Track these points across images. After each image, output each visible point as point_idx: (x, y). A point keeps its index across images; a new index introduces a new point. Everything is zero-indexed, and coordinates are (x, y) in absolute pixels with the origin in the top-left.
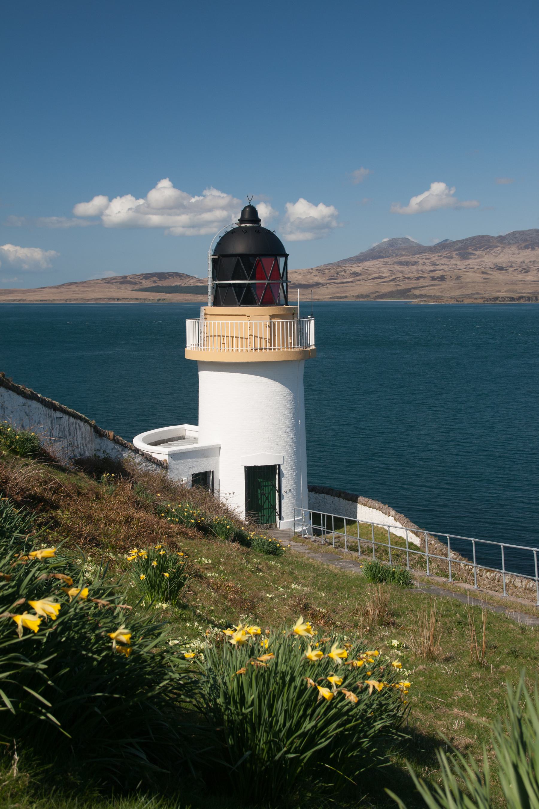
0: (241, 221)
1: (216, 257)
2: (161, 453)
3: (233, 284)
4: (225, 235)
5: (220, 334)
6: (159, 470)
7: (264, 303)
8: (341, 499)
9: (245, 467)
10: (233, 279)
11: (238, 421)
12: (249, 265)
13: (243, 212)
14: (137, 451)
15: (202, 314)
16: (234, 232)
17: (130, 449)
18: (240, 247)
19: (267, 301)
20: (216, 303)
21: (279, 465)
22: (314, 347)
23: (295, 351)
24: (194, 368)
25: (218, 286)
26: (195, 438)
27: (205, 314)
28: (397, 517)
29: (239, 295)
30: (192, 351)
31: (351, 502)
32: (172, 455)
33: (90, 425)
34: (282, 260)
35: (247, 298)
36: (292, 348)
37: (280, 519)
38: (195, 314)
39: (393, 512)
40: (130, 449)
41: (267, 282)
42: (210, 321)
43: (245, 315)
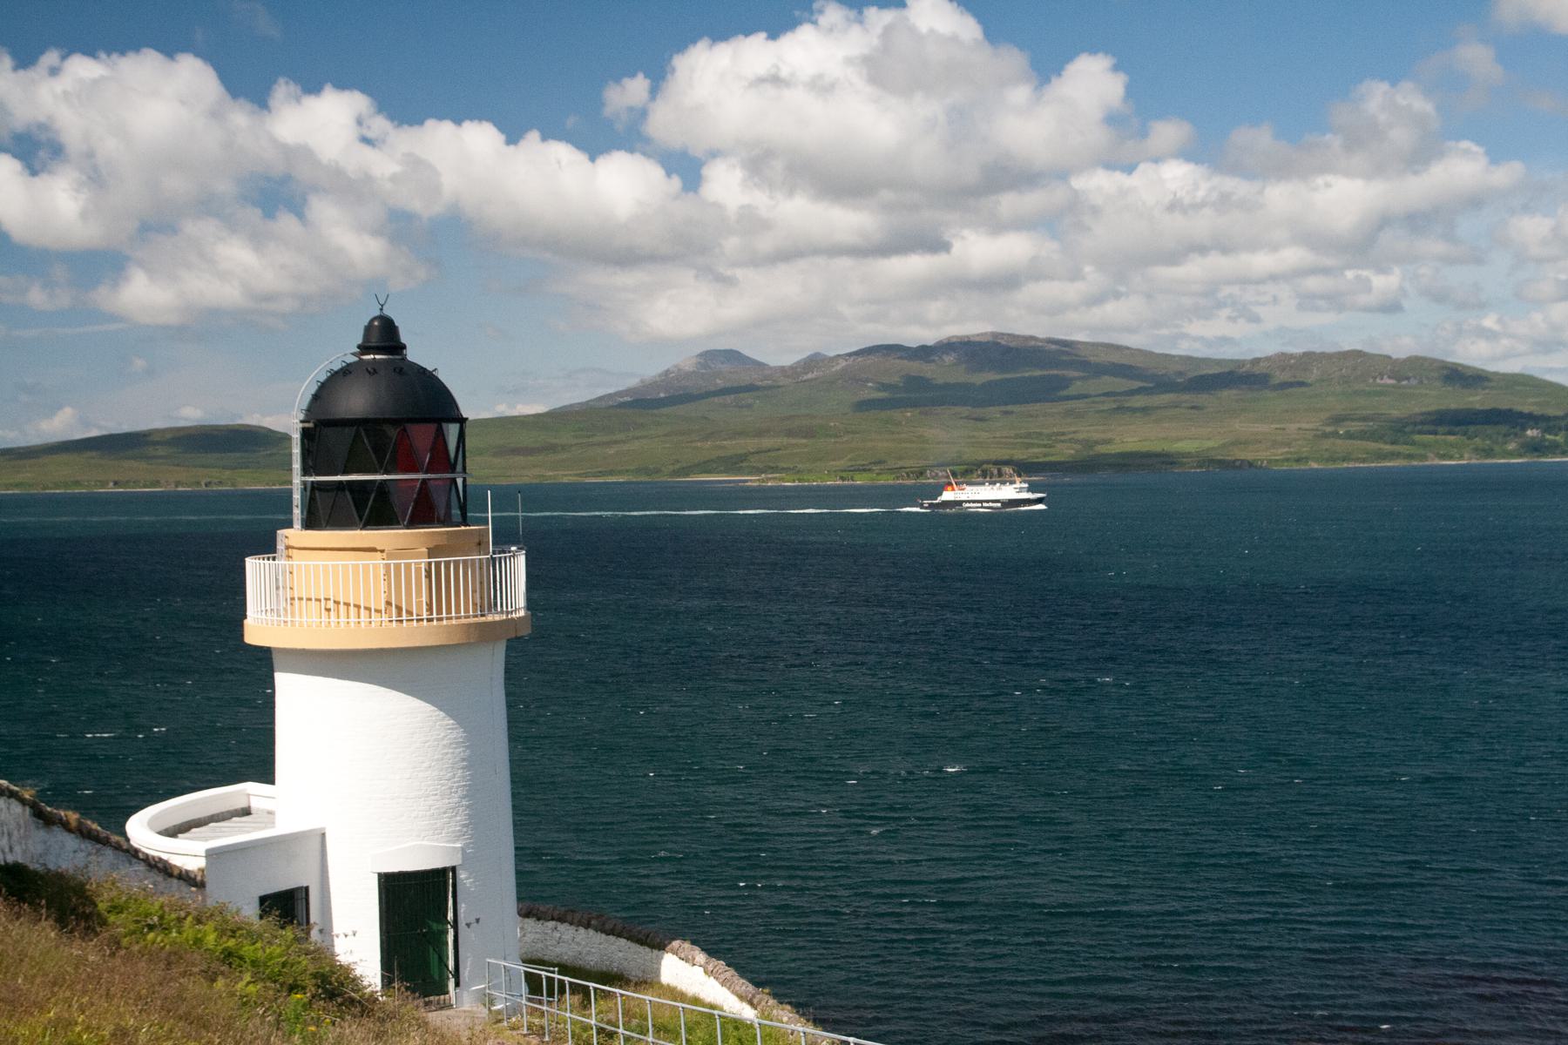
0: (364, 348)
1: (310, 425)
2: (188, 854)
3: (348, 482)
4: (329, 380)
5: (311, 589)
6: (190, 896)
7: (412, 524)
8: (591, 932)
9: (380, 875)
10: (345, 473)
11: (359, 777)
12: (386, 443)
13: (368, 329)
14: (134, 854)
15: (280, 546)
16: (346, 371)
17: (117, 847)
18: (356, 402)
19: (423, 513)
20: (310, 523)
21: (454, 869)
22: (522, 613)
23: (469, 625)
24: (263, 662)
25: (316, 487)
26: (270, 813)
27: (288, 547)
28: (710, 968)
29: (360, 506)
30: (259, 629)
31: (611, 937)
32: (211, 854)
33: (23, 801)
34: (452, 431)
35: (373, 509)
36: (440, 619)
37: (457, 984)
38: (267, 547)
39: (701, 957)
40: (117, 847)
41: (421, 476)
42: (300, 561)
43: (374, 550)
